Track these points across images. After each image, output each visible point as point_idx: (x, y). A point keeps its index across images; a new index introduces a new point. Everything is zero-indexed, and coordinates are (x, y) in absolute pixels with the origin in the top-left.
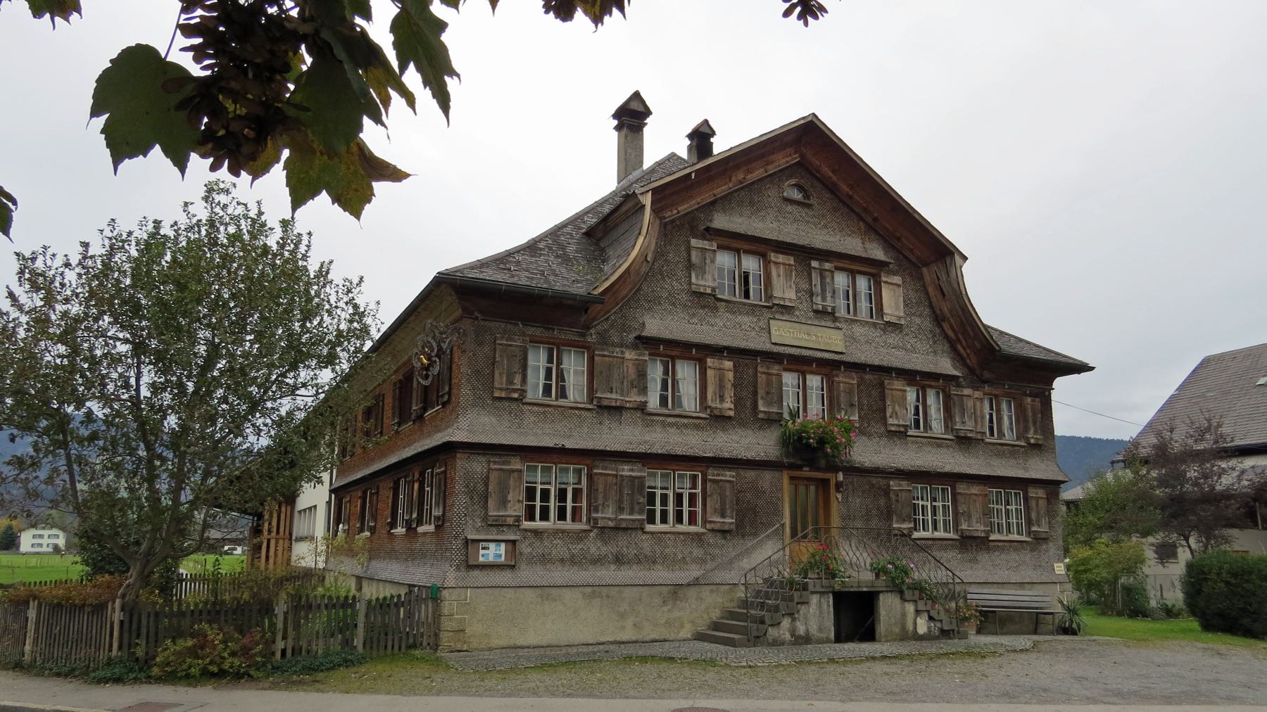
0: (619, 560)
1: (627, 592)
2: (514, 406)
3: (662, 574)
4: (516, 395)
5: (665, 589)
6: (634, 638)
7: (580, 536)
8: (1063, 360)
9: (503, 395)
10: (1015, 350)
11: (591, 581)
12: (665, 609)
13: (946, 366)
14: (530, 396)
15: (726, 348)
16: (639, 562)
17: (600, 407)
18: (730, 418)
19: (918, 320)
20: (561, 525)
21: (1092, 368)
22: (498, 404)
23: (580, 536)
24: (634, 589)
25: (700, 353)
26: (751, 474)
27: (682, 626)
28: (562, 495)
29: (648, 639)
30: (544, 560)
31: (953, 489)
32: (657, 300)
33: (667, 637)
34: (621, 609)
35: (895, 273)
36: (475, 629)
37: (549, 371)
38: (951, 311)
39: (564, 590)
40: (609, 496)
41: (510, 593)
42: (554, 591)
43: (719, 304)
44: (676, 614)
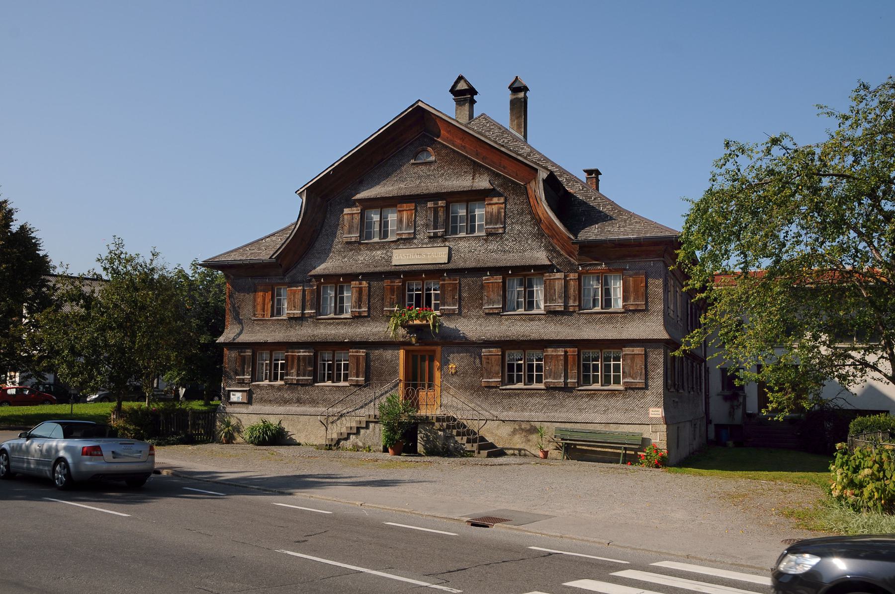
0: (299, 401)
23: (280, 388)
25: (351, 277)
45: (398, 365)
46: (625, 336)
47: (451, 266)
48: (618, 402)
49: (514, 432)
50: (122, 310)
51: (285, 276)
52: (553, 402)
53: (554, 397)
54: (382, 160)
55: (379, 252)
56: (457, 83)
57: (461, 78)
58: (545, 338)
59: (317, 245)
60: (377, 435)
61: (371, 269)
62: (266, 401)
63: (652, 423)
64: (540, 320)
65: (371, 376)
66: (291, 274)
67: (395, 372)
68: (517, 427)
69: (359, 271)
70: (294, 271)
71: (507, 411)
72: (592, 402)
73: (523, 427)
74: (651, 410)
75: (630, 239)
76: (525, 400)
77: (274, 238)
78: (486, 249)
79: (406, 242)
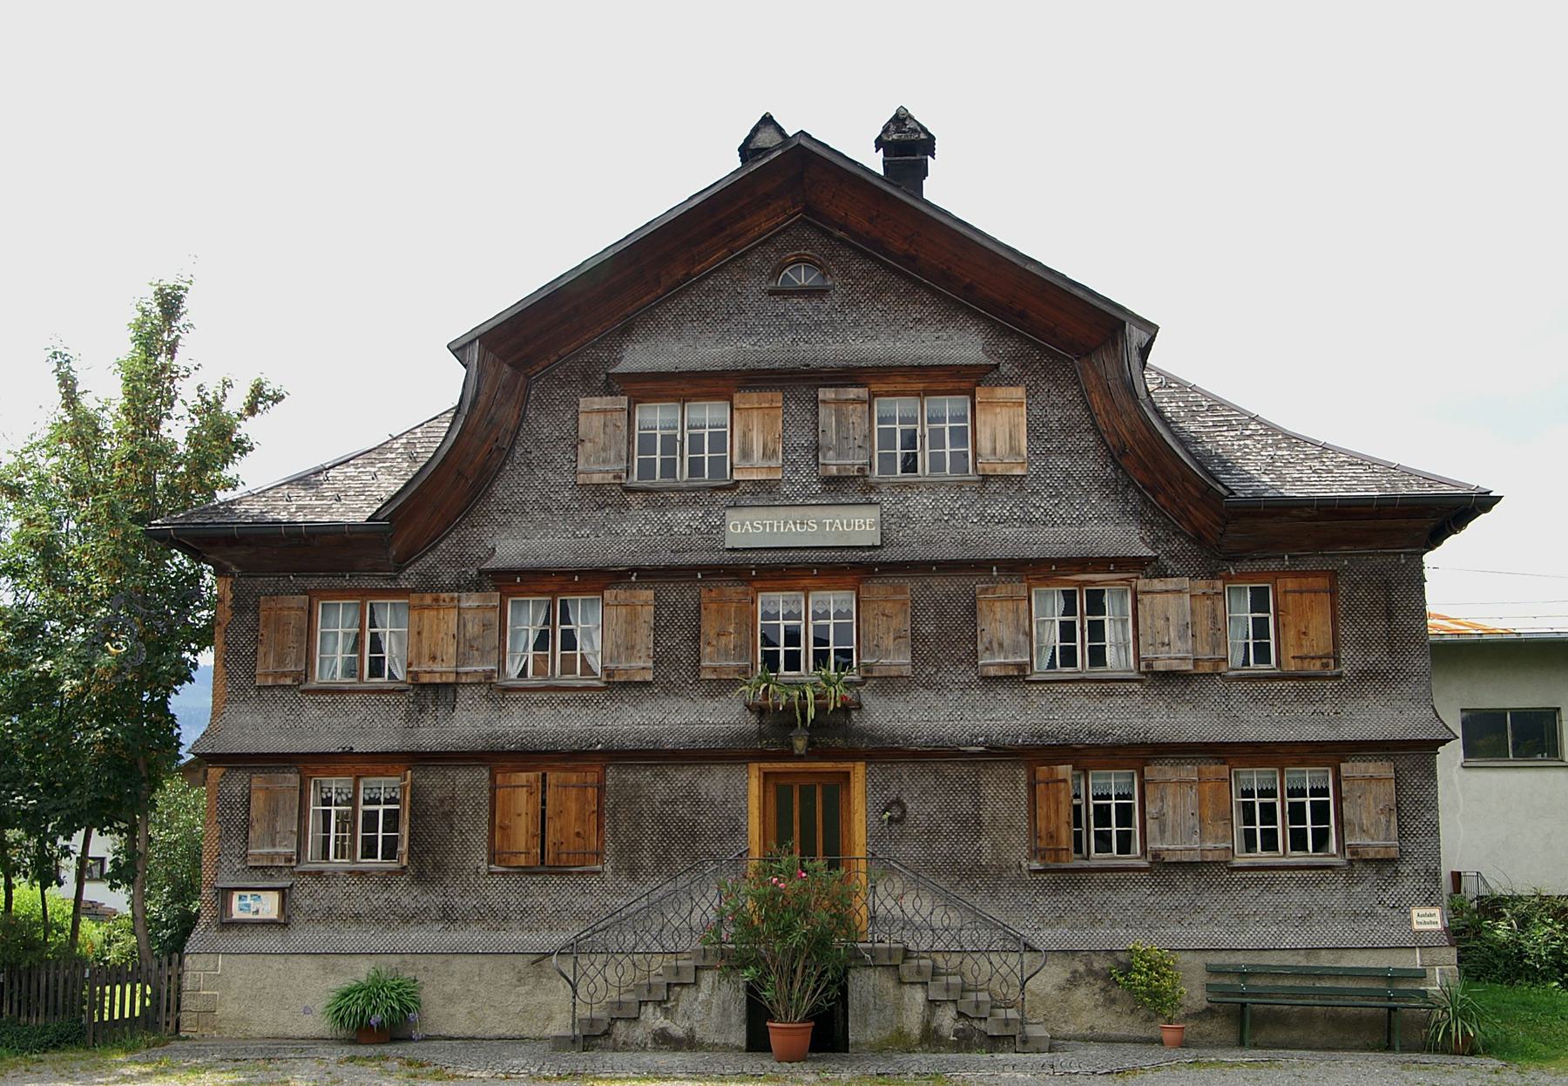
0: (448, 916)
1: (459, 963)
2: (289, 695)
3: (517, 937)
4: (289, 681)
5: (521, 962)
6: (469, 1033)
7: (387, 878)
8: (1446, 489)
9: (270, 682)
10: (1304, 482)
11: (400, 946)
12: (522, 990)
13: (1128, 539)
14: (320, 677)
15: (936, 563)
16: (482, 919)
17: (985, 678)
18: (646, 684)
19: (1063, 463)
20: (1297, 858)
21: (1482, 503)
22: (266, 694)
23: (387, 878)
24: (470, 959)
25: (597, 579)
26: (683, 777)
27: (550, 1018)
28: (1297, 813)
29: (492, 1034)
30: (329, 916)
31: (1142, 775)
32: (520, 509)
33: (525, 1033)
34: (448, 989)
35: (1012, 382)
36: (229, 1009)
37: (1067, 631)
38: (1132, 433)
39: (359, 959)
40: (432, 817)
41: (277, 963)
42: (342, 960)
43: (630, 498)
44: (541, 997)
45: (744, 812)
46: (1348, 732)
47: (887, 555)
48: (1334, 896)
49: (1074, 981)
50: (266, 675)
51: (400, 569)
52: (1169, 899)
53: (1172, 886)
54: (688, 276)
55: (682, 515)
56: (755, 130)
57: (767, 120)
58: (1176, 739)
59: (499, 490)
60: (713, 1006)
61: (665, 558)
62: (344, 919)
63: (1422, 942)
64: (1127, 694)
65: (685, 843)
66: (421, 566)
67: (737, 829)
68: (1082, 968)
69: (630, 561)
70: (430, 559)
71: (1051, 926)
72: (1268, 897)
73: (1096, 966)
74: (1415, 912)
75: (1372, 498)
76: (1098, 897)
77: (351, 471)
78: (982, 517)
79: (765, 493)
